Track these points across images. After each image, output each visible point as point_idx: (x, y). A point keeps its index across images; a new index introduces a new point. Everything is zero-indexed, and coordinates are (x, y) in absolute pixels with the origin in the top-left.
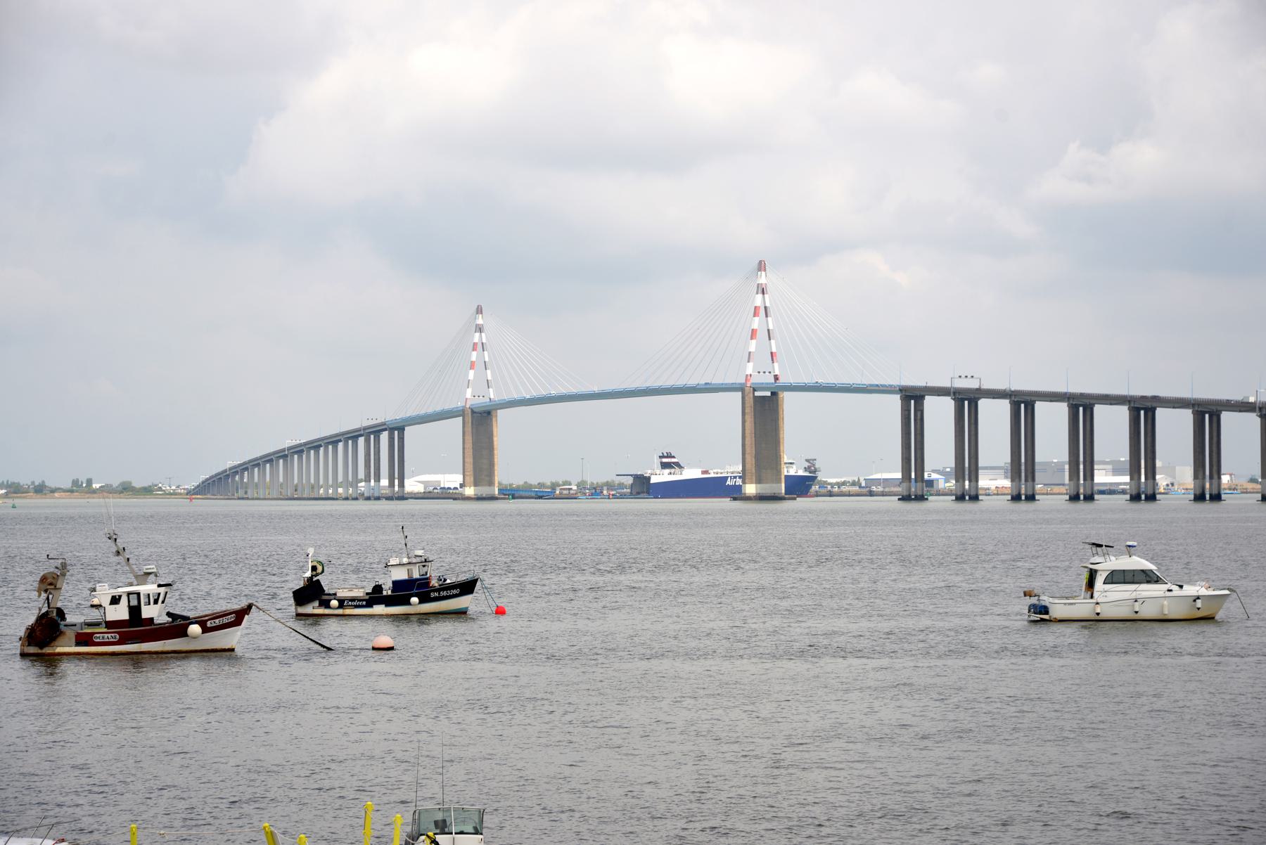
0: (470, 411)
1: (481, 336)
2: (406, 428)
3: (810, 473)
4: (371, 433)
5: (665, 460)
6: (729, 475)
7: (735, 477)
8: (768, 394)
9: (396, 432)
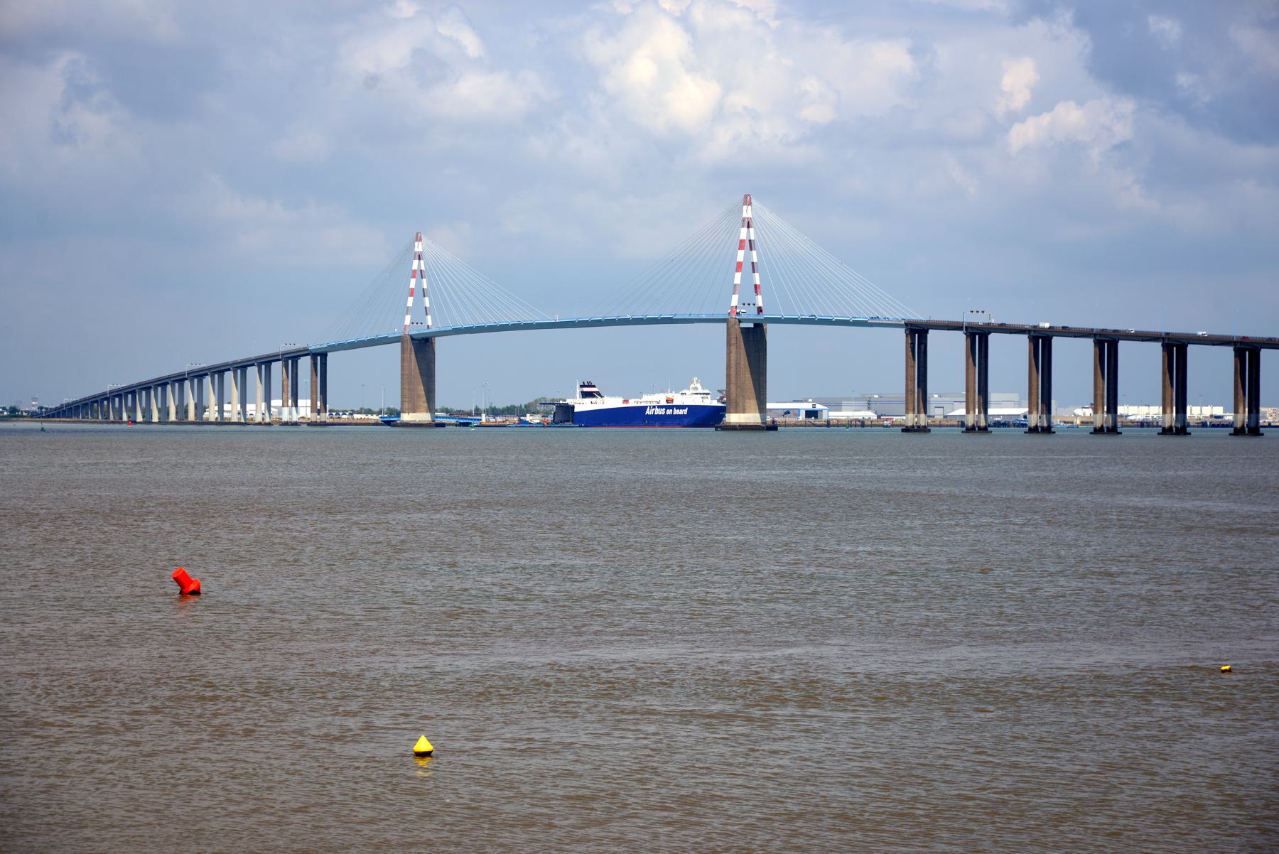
0: (409, 338)
1: (749, 232)
2: (329, 354)
3: (723, 403)
4: (289, 358)
5: (586, 389)
6: (649, 404)
7: (654, 407)
8: (751, 325)
9: (319, 358)
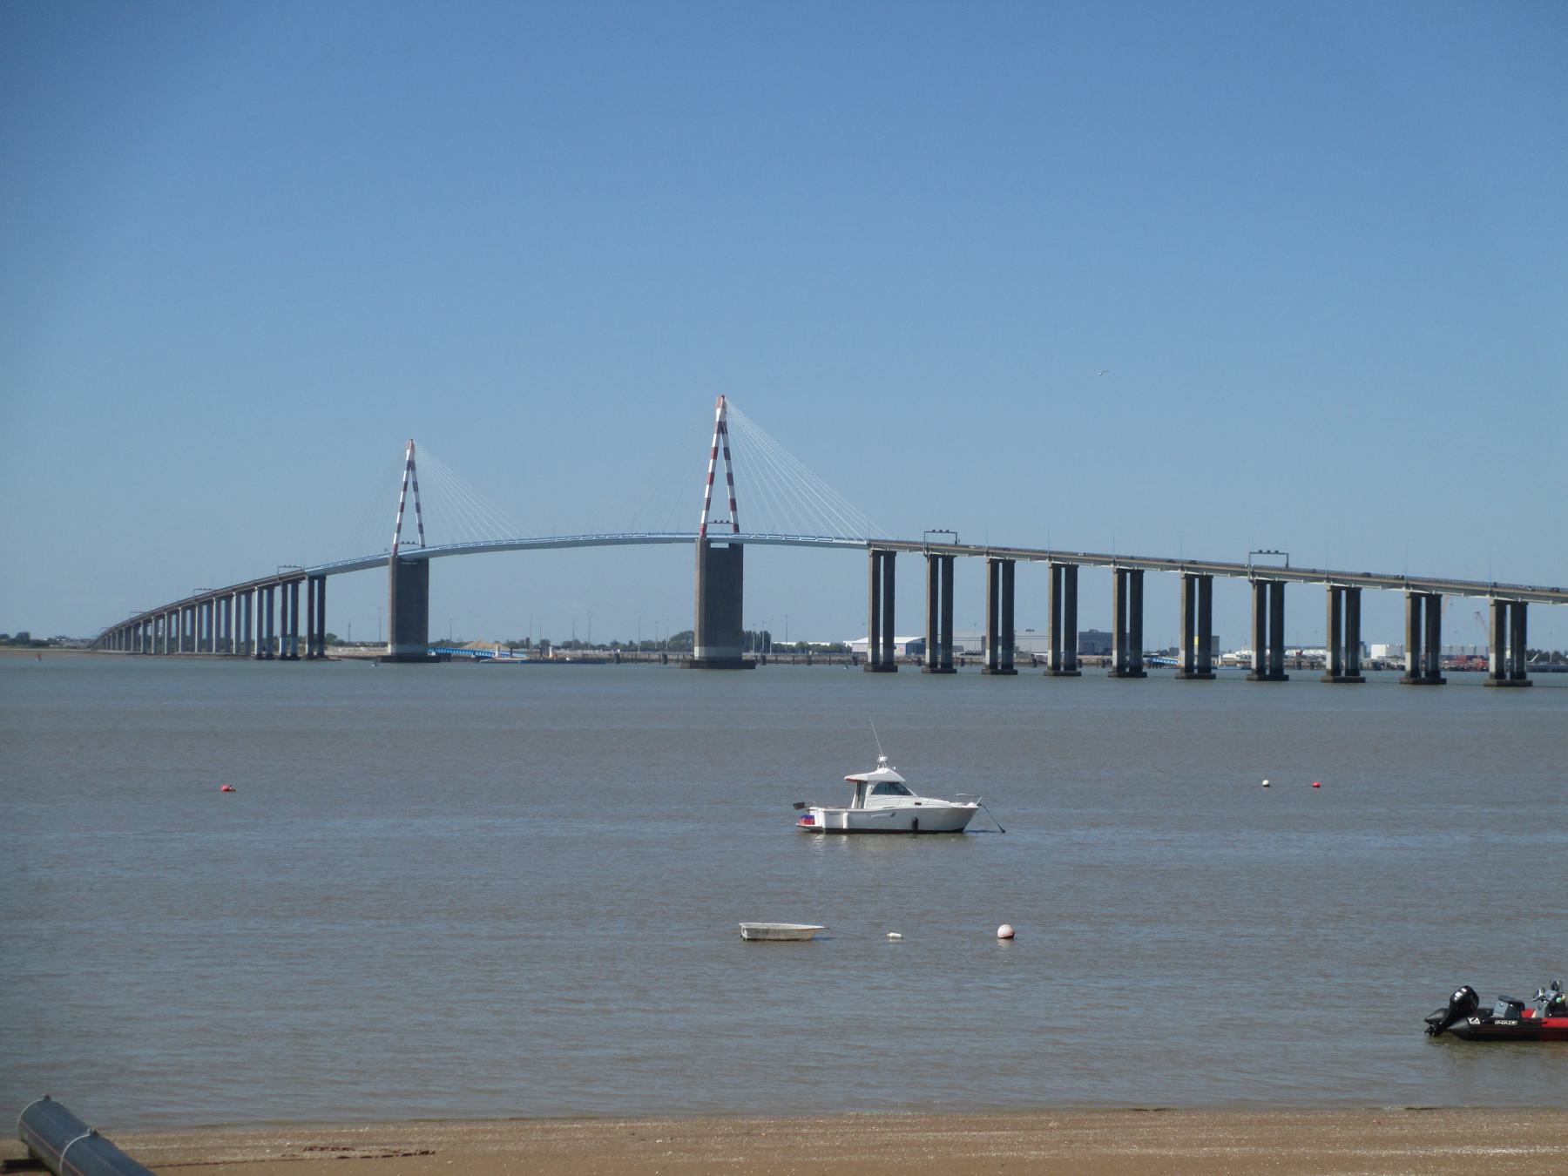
8: (726, 546)
